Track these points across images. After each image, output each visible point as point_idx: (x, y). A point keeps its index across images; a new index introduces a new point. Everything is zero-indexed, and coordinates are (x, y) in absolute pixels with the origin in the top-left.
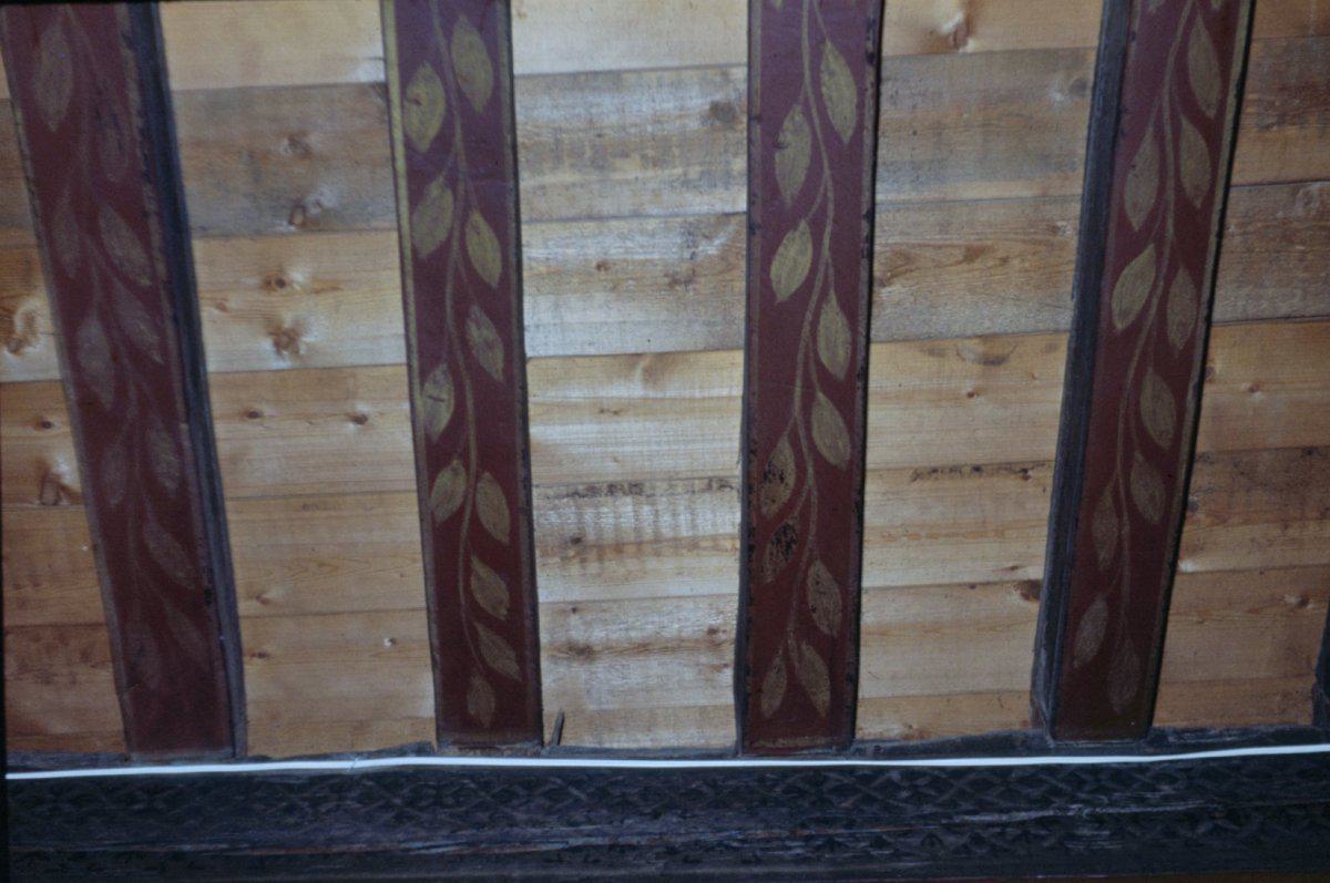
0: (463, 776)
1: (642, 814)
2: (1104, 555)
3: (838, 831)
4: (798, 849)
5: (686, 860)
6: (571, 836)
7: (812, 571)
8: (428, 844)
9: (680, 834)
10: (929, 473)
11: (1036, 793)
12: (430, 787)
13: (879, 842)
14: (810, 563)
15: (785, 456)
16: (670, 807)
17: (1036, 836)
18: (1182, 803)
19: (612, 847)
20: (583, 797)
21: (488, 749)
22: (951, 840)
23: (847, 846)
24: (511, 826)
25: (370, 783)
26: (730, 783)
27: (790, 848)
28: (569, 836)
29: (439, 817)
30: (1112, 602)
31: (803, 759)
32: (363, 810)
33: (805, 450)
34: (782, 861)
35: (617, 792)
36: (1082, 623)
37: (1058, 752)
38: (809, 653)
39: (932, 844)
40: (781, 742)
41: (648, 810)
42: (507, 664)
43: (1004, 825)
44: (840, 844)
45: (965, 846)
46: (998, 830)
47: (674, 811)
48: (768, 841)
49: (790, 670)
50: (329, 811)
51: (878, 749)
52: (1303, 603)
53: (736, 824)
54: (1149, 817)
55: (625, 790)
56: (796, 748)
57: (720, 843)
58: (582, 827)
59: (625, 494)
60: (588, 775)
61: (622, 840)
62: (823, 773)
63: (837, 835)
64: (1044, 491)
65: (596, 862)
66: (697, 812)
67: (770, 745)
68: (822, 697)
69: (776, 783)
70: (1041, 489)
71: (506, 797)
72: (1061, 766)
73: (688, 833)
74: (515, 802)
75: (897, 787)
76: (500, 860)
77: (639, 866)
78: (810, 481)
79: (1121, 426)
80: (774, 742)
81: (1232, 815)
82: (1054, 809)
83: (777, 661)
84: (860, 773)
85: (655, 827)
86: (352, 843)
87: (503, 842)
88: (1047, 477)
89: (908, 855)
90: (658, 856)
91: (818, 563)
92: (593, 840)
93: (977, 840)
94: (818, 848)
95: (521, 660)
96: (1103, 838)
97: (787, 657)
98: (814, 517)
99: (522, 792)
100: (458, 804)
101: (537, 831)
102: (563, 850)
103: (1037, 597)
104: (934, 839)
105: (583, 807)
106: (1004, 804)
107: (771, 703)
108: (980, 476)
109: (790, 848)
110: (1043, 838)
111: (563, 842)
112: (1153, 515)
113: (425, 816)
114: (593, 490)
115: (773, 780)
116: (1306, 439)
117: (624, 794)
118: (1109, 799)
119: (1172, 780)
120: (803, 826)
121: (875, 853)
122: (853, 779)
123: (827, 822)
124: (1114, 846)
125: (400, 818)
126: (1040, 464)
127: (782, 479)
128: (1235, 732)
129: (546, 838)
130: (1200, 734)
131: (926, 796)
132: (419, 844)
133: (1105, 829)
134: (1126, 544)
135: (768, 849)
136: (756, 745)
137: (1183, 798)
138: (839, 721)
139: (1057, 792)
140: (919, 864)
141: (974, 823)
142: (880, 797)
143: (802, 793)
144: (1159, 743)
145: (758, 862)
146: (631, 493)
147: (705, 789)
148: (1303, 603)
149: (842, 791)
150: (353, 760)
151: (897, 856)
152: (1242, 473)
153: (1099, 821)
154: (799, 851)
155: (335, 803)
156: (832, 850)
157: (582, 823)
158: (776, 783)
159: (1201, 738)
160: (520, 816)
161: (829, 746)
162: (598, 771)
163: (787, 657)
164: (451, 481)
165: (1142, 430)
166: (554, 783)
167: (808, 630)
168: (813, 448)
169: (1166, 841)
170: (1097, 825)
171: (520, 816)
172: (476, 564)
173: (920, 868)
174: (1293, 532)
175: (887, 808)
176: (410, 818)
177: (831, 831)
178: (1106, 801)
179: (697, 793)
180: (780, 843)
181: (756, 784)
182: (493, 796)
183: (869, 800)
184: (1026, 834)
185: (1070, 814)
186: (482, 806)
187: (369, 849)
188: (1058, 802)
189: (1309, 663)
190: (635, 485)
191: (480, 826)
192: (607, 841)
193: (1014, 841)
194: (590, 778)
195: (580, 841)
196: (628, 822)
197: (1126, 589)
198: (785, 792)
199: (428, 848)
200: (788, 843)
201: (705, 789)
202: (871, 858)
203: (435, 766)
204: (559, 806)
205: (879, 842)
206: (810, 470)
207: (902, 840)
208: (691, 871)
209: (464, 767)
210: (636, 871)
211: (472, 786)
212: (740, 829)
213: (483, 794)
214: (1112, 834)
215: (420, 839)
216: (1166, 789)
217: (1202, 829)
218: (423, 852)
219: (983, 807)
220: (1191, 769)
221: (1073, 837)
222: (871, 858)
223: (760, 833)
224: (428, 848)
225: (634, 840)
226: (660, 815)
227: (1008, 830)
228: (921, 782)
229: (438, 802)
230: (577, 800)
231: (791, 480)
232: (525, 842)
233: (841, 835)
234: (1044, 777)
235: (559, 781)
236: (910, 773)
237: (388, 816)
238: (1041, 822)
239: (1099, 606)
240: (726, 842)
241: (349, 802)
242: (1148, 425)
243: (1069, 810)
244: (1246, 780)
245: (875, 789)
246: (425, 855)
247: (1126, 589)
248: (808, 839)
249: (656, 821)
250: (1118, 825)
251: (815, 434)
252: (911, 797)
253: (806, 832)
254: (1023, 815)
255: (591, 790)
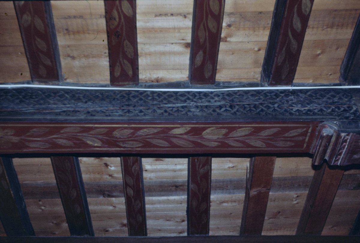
0: (39, 90)
1: (83, 102)
2: (202, 40)
3: (131, 108)
4: (120, 112)
5: (92, 115)
6: (64, 108)
7: (125, 43)
8: (27, 109)
9: (91, 108)
10: (159, 15)
11: (183, 99)
12: (30, 93)
13: (141, 111)
14: (124, 40)
15: (115, 14)
16: (90, 100)
17: (180, 111)
18: (219, 103)
19: (73, 111)
20: (68, 97)
21: (46, 83)
22: (159, 111)
23: (133, 112)
24: (49, 104)
25: (14, 91)
26: (106, 94)
27: (118, 112)
28: (63, 108)
29: (31, 101)
30: (205, 53)
31: (126, 88)
32: (11, 99)
33: (121, 13)
34: (116, 116)
35: (77, 96)
36: (197, 57)
37: (191, 88)
38: (126, 62)
39: (154, 112)
40: (121, 83)
41: (84, 101)
42: (49, 63)
43: (173, 108)
44: (131, 111)
45: (162, 113)
46: (171, 109)
47: (91, 101)
48: (113, 110)
49: (121, 66)
50: (3, 99)
51: (145, 85)
52: (259, 50)
53: (106, 105)
54: (210, 107)
55: (80, 95)
56: (125, 85)
57: (101, 111)
58: (67, 105)
59: (78, 18)
60: (70, 90)
61: (77, 109)
62: (131, 92)
63: (131, 109)
64: (190, 20)
65: (69, 115)
66: (96, 102)
67: (117, 84)
68: (130, 73)
69: (118, 94)
70: (189, 20)
71: (49, 96)
72: (191, 91)
73: (93, 108)
74: (51, 98)
75: (149, 96)
76: (45, 114)
77: (80, 116)
78: (123, 20)
79: (205, 8)
80: (119, 83)
81: (231, 107)
82: (187, 103)
83: (118, 64)
84: (140, 92)
85: (85, 106)
86: (8, 108)
87: (46, 109)
88: (191, 17)
89: (148, 115)
90: (85, 114)
91: (126, 40)
92: (69, 109)
93: (166, 111)
94: (126, 112)
95: (52, 62)
96: (197, 112)
97: (120, 63)
98: (124, 29)
99: (53, 95)
100: (37, 98)
101: (55, 106)
102: (61, 112)
103: (189, 47)
104: (155, 111)
105: (68, 100)
106: (174, 101)
107: (117, 74)
108: (173, 16)
109: (118, 112)
110: (182, 111)
111: (60, 109)
112: (214, 31)
113: (27, 101)
114: (70, 17)
115: (118, 93)
116: (260, 10)
117: (79, 96)
118: (201, 101)
119: (218, 96)
120: (123, 106)
121: (139, 114)
122: (138, 93)
123: (128, 105)
124: (199, 114)
125: (21, 101)
126: (189, 14)
127: (115, 19)
128: (238, 83)
129: (57, 108)
130: (229, 83)
131: (155, 99)
132: (25, 109)
133: (198, 109)
134: (207, 38)
135: (113, 113)
136: (114, 84)
137: (219, 101)
138: (134, 79)
139: (189, 99)
140: (150, 117)
141: (166, 107)
142: (144, 99)
143: (124, 97)
144: (218, 85)
145: (110, 116)
146: (80, 18)
147: (100, 95)
148: (259, 50)
149: (134, 97)
150: (11, 85)
151: (145, 115)
152: (243, 18)
153: (197, 107)
154: (121, 113)
155: (5, 97)
156: (129, 113)
157: (67, 104)
158: (118, 94)
159: (229, 84)
160: (52, 102)
161: (133, 84)
162: (73, 90)
163: (120, 63)
164: (27, 18)
165: (211, 11)
166: (62, 93)
167: (125, 57)
168: (122, 11)
169: (213, 113)
170: (196, 108)
171: (52, 102)
172: (36, 38)
173: (150, 119)
174: (256, 33)
175: (145, 102)
176: (23, 101)
177: (129, 108)
178: (200, 102)
179: (97, 97)
180: (116, 111)
181: (113, 94)
182: (45, 96)
183: (141, 99)
184: (178, 110)
185: (191, 105)
186: (42, 99)
187: (12, 110)
188: (188, 101)
189: (261, 64)
190: (81, 16)
191: (41, 104)
192: (72, 109)
193: (174, 112)
194: (71, 91)
195: (66, 109)
196: (79, 104)
197: (208, 49)
198: (120, 97)
199: (26, 110)
200: (118, 111)
201: (100, 95)
202: (138, 115)
203: (32, 87)
204: (62, 99)
205: (141, 111)
206: (122, 18)
207: (147, 111)
208: (92, 118)
209: (38, 88)
210: (79, 118)
211: (41, 93)
212: (106, 107)
213: (43, 95)
214: (200, 111)
215: (26, 108)
216: (216, 98)
217: (223, 109)
218: (25, 111)
219: (169, 102)
220: (224, 93)
221: (190, 111)
222: (138, 115)
223: (112, 108)
224: (26, 110)
225: (79, 109)
226: (87, 102)
227: (174, 109)
228: (155, 95)
229: (31, 97)
230: (67, 98)
231: (117, 20)
232: (52, 109)
233: (131, 109)
234: (186, 94)
235: (63, 92)
236: (153, 92)
237: (18, 101)
238: (183, 107)
239: (201, 53)
240: (102, 110)
241: (8, 97)
242: (212, 8)
243: (190, 103)
244: (237, 96)
245: (143, 97)
246: (25, 112)
247: (208, 49)
248: (123, 110)
249: (85, 104)
250: (202, 108)
251: (123, 9)
252: (152, 99)
253: (123, 108)
254: (179, 105)
255: (71, 95)
